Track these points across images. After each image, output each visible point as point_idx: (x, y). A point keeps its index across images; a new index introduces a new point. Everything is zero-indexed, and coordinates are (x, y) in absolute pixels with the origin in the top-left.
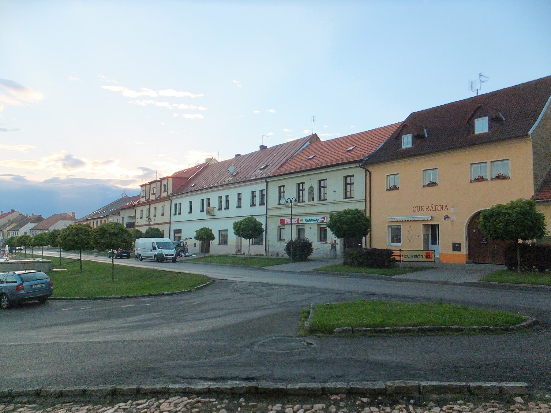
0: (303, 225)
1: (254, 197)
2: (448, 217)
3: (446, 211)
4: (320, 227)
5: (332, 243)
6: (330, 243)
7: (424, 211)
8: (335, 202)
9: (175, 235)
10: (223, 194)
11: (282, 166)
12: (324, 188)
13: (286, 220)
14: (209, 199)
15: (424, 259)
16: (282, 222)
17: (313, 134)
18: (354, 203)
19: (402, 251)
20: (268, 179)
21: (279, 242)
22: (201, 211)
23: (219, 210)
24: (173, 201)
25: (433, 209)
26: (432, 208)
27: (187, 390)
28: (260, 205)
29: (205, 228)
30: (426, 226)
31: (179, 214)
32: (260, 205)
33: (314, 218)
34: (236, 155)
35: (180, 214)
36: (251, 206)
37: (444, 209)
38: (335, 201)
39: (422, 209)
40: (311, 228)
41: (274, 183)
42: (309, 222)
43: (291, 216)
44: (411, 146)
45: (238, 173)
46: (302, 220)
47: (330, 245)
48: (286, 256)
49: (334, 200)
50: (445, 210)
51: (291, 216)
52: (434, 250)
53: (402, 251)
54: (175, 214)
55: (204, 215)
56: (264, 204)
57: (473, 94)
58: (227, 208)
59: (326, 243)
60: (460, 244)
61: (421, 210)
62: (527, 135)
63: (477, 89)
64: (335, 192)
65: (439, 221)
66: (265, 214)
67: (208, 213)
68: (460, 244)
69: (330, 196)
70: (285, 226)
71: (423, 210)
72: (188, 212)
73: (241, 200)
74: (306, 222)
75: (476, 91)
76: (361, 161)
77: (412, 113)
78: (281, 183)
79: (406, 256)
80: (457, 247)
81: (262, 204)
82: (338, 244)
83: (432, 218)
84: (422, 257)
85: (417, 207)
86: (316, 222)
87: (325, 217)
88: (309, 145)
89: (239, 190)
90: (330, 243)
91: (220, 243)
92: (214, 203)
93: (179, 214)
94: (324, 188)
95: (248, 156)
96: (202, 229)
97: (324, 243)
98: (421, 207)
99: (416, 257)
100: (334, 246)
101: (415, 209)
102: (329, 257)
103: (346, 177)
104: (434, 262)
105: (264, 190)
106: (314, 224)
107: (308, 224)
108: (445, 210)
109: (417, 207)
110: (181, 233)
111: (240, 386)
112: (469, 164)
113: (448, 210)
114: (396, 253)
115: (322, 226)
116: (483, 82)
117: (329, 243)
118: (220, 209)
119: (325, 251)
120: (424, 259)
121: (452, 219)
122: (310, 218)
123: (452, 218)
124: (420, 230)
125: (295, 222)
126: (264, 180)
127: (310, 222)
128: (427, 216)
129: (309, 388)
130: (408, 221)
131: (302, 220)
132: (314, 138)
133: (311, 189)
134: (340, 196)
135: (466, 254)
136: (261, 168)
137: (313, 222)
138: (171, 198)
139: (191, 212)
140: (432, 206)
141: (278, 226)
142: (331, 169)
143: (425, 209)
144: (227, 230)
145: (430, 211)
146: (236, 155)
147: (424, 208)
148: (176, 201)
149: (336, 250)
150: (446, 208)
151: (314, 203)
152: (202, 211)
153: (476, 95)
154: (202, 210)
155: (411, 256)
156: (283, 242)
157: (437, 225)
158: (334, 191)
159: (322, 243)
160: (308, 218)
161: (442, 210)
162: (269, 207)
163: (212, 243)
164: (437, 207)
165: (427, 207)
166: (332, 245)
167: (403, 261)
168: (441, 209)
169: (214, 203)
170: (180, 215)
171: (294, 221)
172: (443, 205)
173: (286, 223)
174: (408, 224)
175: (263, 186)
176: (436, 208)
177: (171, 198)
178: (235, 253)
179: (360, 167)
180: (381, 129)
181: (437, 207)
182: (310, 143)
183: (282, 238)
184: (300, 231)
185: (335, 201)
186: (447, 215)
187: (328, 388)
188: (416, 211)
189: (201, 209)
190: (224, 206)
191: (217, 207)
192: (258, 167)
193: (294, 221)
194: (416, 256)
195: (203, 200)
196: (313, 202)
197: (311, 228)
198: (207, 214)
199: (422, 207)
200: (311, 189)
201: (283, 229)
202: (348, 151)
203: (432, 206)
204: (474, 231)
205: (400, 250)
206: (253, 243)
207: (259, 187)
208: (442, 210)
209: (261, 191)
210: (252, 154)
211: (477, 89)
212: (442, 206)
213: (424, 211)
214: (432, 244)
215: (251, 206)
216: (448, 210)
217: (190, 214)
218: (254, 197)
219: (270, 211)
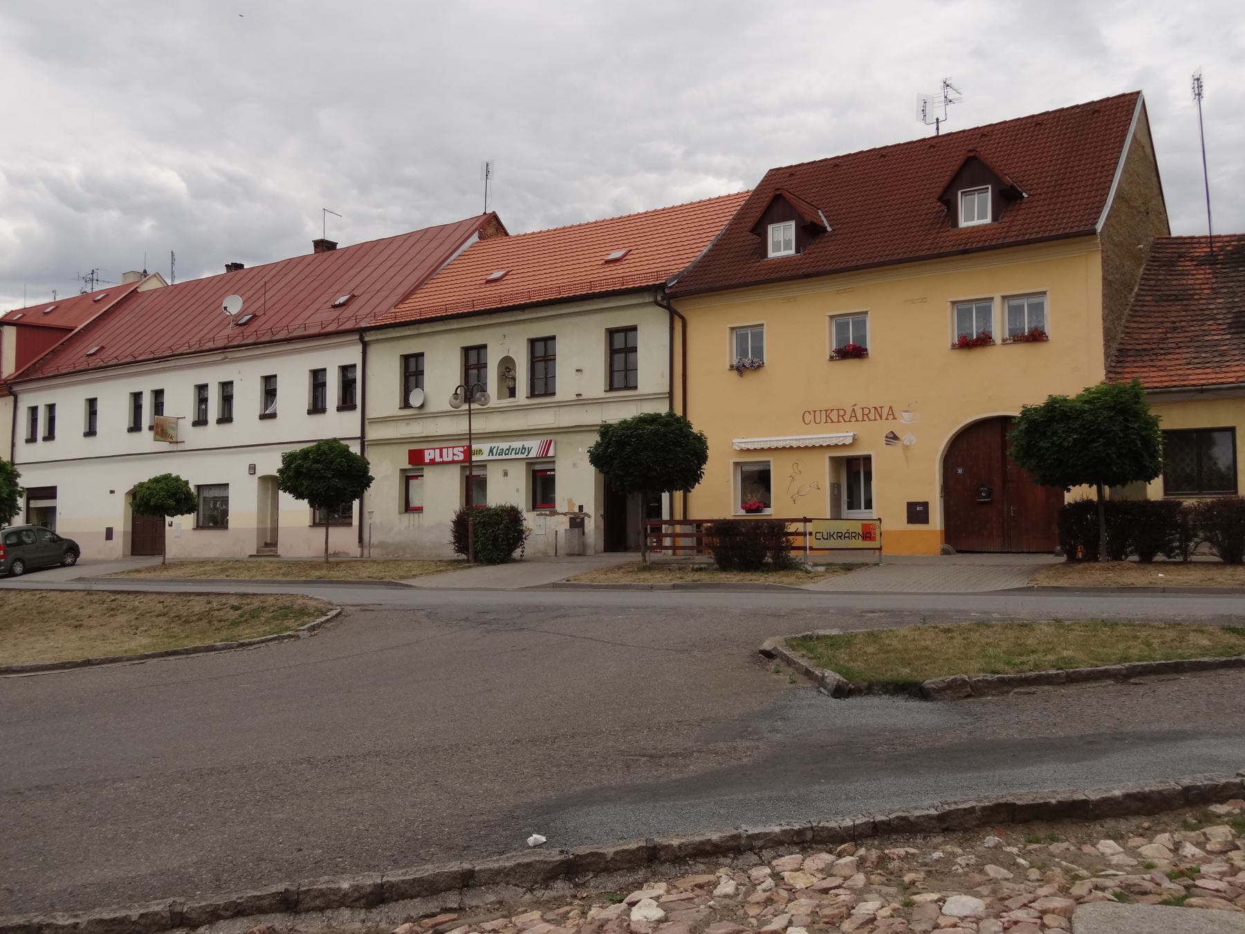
0: (483, 465)
1: (202, 400)
2: (895, 438)
3: (891, 421)
4: (535, 472)
5: (571, 513)
6: (565, 514)
7: (833, 422)
8: (580, 401)
9: (31, 506)
10: (213, 376)
11: (407, 297)
12: (479, 369)
13: (426, 452)
14: (51, 408)
15: (859, 543)
16: (416, 457)
17: (485, 213)
18: (554, 409)
19: (810, 520)
20: (368, 333)
21: (407, 515)
22: (131, 430)
23: (195, 424)
24: (21, 397)
25: (856, 417)
26: (891, 413)
27: (809, 835)
28: (340, 409)
29: (167, 478)
30: (835, 461)
31: (45, 439)
32: (340, 409)
33: (517, 444)
34: (227, 266)
35: (50, 436)
36: (310, 412)
37: (884, 417)
38: (580, 398)
39: (827, 416)
40: (506, 474)
41: (387, 345)
42: (500, 457)
43: (470, 439)
44: (792, 252)
45: (254, 317)
46: (480, 452)
47: (566, 520)
48: (453, 555)
49: (577, 395)
50: (887, 419)
51: (470, 439)
52: (880, 519)
53: (810, 520)
54: (32, 439)
55: (146, 440)
56: (353, 408)
57: (929, 132)
58: (226, 418)
59: (554, 513)
60: (925, 505)
61: (824, 420)
62: (1094, 232)
63: (937, 119)
64: (579, 373)
65: (871, 445)
66: (360, 435)
67: (161, 431)
68: (925, 505)
69: (566, 384)
70: (423, 469)
71: (829, 420)
72: (336, 405)
73: (275, 395)
74: (491, 458)
75: (935, 126)
76: (662, 287)
77: (770, 170)
78: (411, 347)
79: (819, 536)
80: (917, 513)
81: (346, 403)
82: (589, 516)
83: (855, 439)
84: (840, 537)
85: (815, 412)
86: (524, 456)
87: (551, 441)
88: (477, 243)
89: (268, 366)
90: (565, 514)
91: (201, 524)
92: (180, 404)
93: (45, 439)
94: (479, 369)
95: (277, 269)
96: (157, 480)
97: (546, 515)
98: (823, 413)
99: (840, 537)
100: (578, 520)
101: (808, 418)
102: (561, 552)
103: (611, 333)
104: (880, 549)
105: (354, 366)
106: (516, 463)
107: (505, 462)
108: (887, 419)
109: (815, 412)
110: (54, 497)
111: (960, 807)
112: (949, 303)
113: (894, 418)
114: (792, 528)
115: (538, 467)
116: (950, 101)
117: (562, 514)
118: (201, 421)
119: (551, 537)
120: (859, 543)
121: (907, 442)
122: (504, 445)
123: (906, 438)
124: (821, 474)
125: (456, 458)
126: (358, 337)
127: (504, 457)
128: (841, 435)
129: (1152, 792)
130: (791, 447)
131: (480, 452)
132: (491, 225)
133: (507, 366)
134: (595, 383)
135: (941, 531)
136: (337, 303)
137: (513, 456)
138: (15, 389)
139: (91, 432)
140: (853, 409)
141: (402, 470)
142: (546, 311)
143: (834, 416)
144: (228, 484)
145: (850, 421)
146: (227, 266)
147: (833, 416)
148: (37, 398)
149: (584, 534)
150: (853, 415)
151: (515, 404)
152: (136, 427)
153: (934, 134)
154: (132, 425)
155: (830, 536)
156: (416, 515)
157: (868, 459)
158: (577, 370)
159: (541, 514)
160: (497, 445)
161: (881, 417)
162: (370, 414)
163: (171, 525)
164: (866, 411)
165: (842, 413)
166: (571, 519)
167: (811, 548)
168: (878, 417)
169: (180, 404)
170: (49, 444)
171: (454, 454)
172: (881, 407)
173: (427, 460)
174: (789, 459)
175: (351, 354)
176: (863, 415)
177: (15, 389)
178: (255, 553)
179: (657, 303)
180: (708, 202)
181: (866, 411)
182: (480, 238)
183: (411, 505)
184: (474, 484)
185: (580, 398)
186: (892, 432)
187: (1093, 801)
188: (813, 422)
189: (27, 435)
190: (41, 430)
191: (190, 413)
192: (322, 300)
193: (454, 454)
194: (840, 535)
195: (137, 397)
196: (511, 399)
197: (506, 474)
198: (158, 438)
199: (829, 412)
200: (507, 366)
201: (416, 477)
202: (607, 262)
203: (853, 409)
204: (960, 471)
205: (806, 520)
206: (317, 521)
207: (332, 359)
208: (881, 417)
209: (346, 370)
210: (290, 263)
211: (937, 119)
212: (879, 409)
213: (833, 422)
214: (848, 509)
215: (310, 412)
216: (894, 418)
217: (90, 440)
218: (202, 400)
219: (374, 426)
